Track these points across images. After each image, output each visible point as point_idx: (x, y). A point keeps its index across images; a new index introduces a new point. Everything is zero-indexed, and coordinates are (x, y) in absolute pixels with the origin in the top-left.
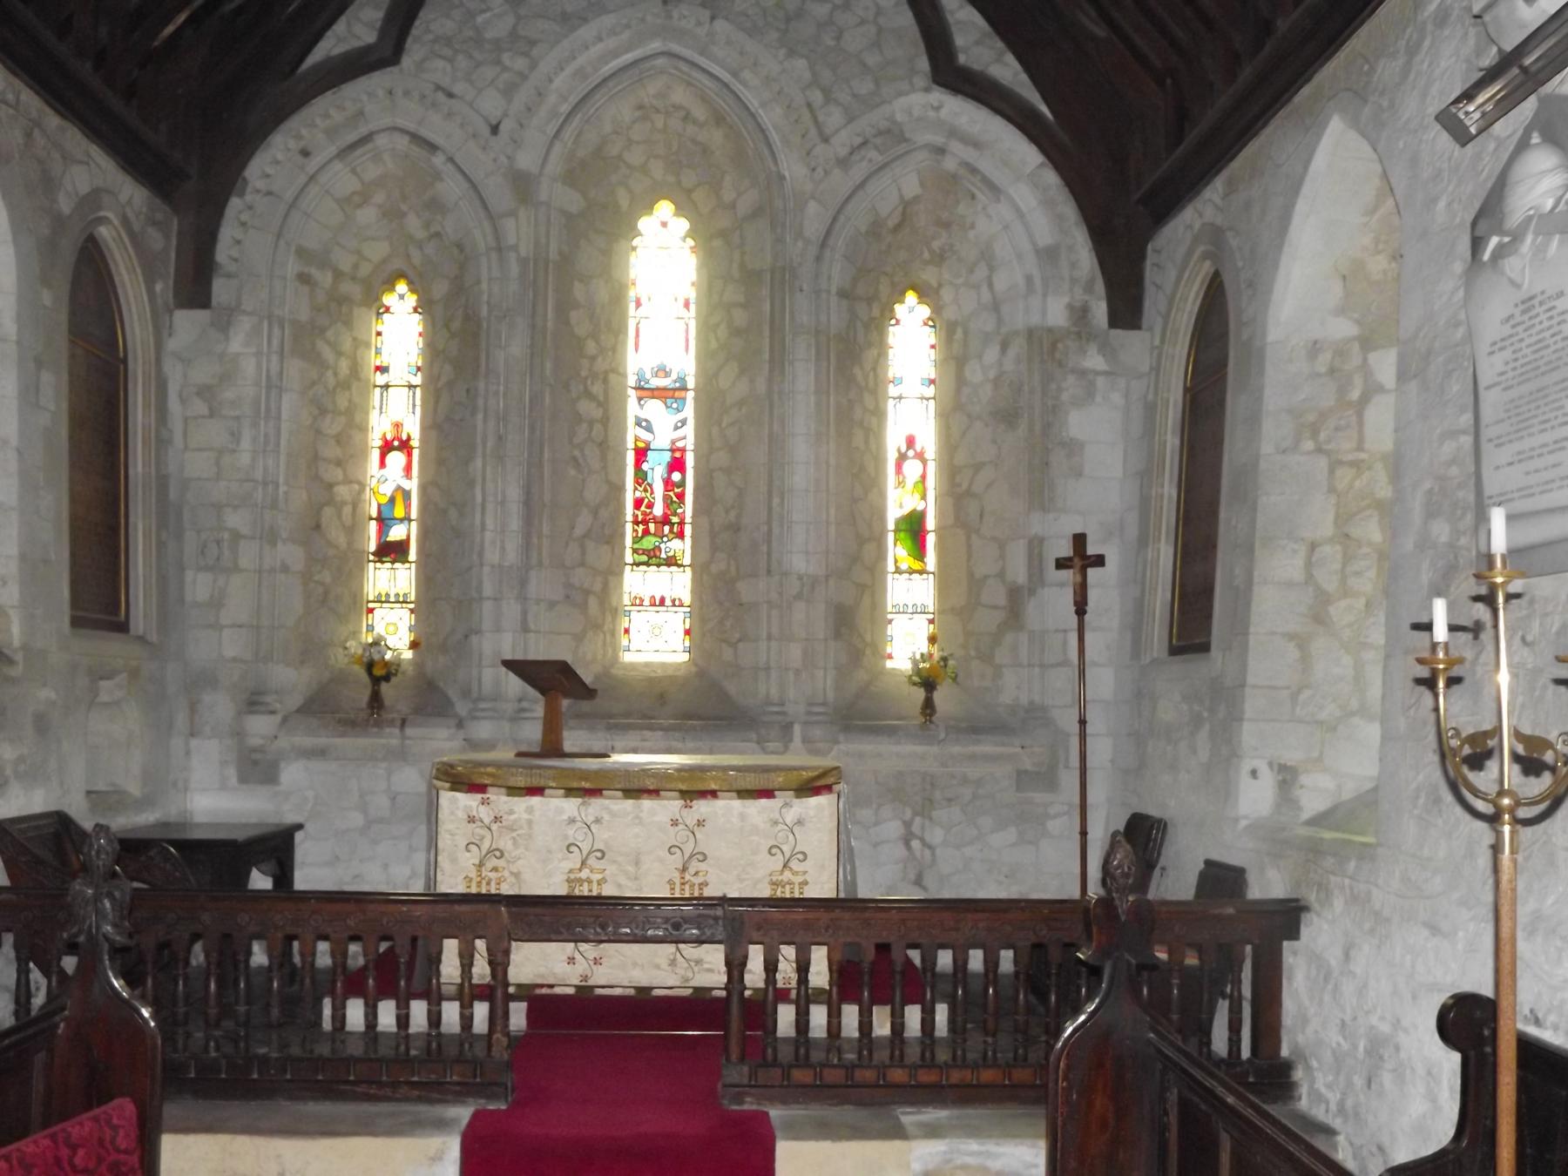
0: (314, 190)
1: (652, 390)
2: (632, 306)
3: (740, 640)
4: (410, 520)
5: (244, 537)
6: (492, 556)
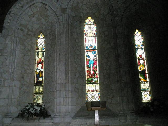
0: (24, 13)
1: (89, 50)
2: (85, 35)
3: (112, 98)
4: (43, 77)
5: (7, 79)
6: (59, 81)
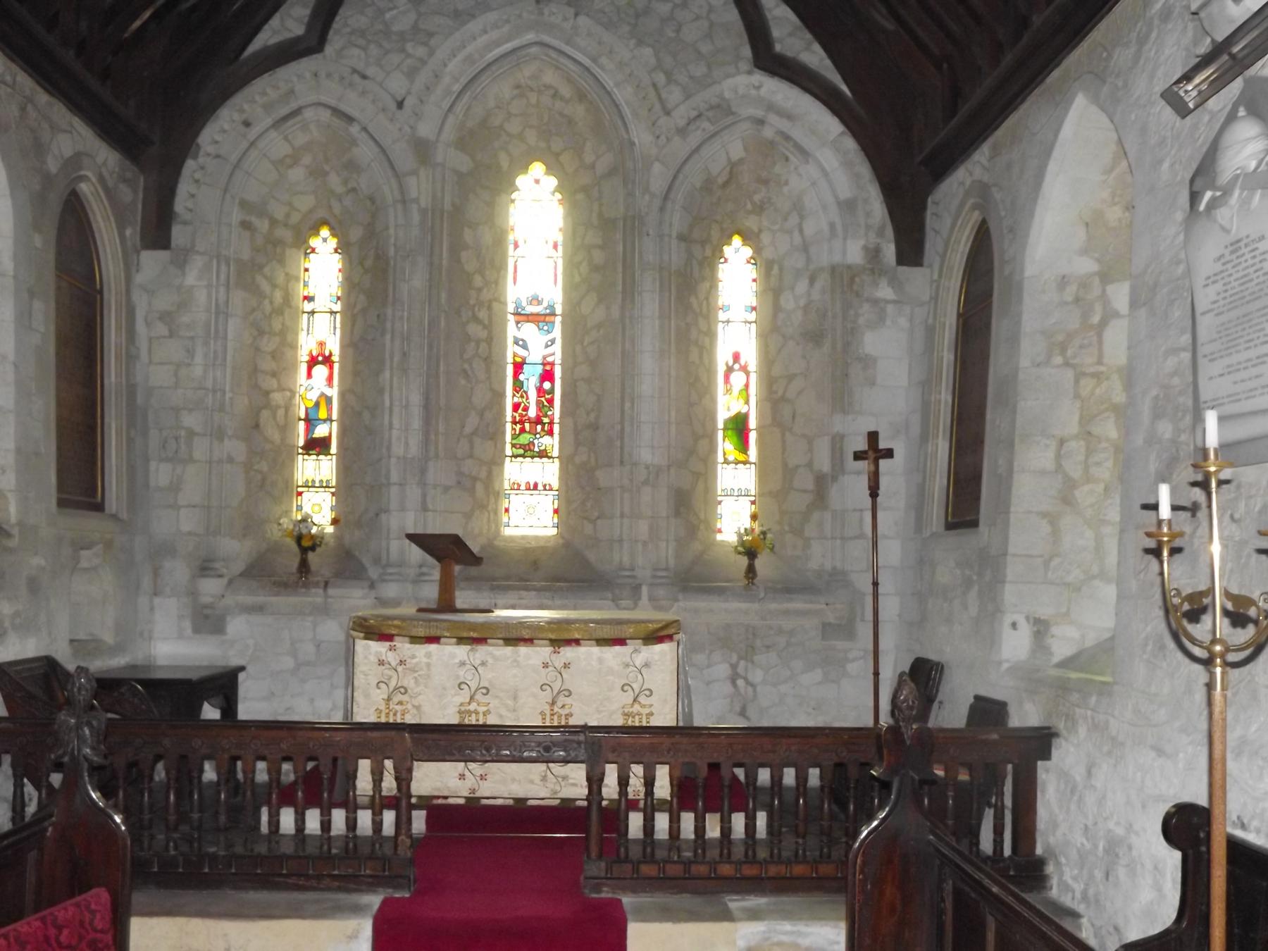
0: (254, 154)
1: (527, 315)
2: (511, 247)
4: (332, 421)
5: (197, 434)
6: (398, 449)
